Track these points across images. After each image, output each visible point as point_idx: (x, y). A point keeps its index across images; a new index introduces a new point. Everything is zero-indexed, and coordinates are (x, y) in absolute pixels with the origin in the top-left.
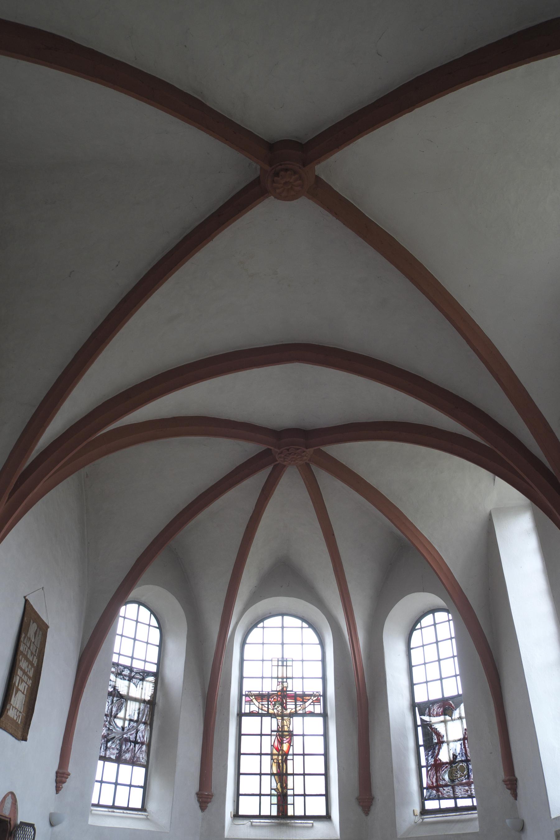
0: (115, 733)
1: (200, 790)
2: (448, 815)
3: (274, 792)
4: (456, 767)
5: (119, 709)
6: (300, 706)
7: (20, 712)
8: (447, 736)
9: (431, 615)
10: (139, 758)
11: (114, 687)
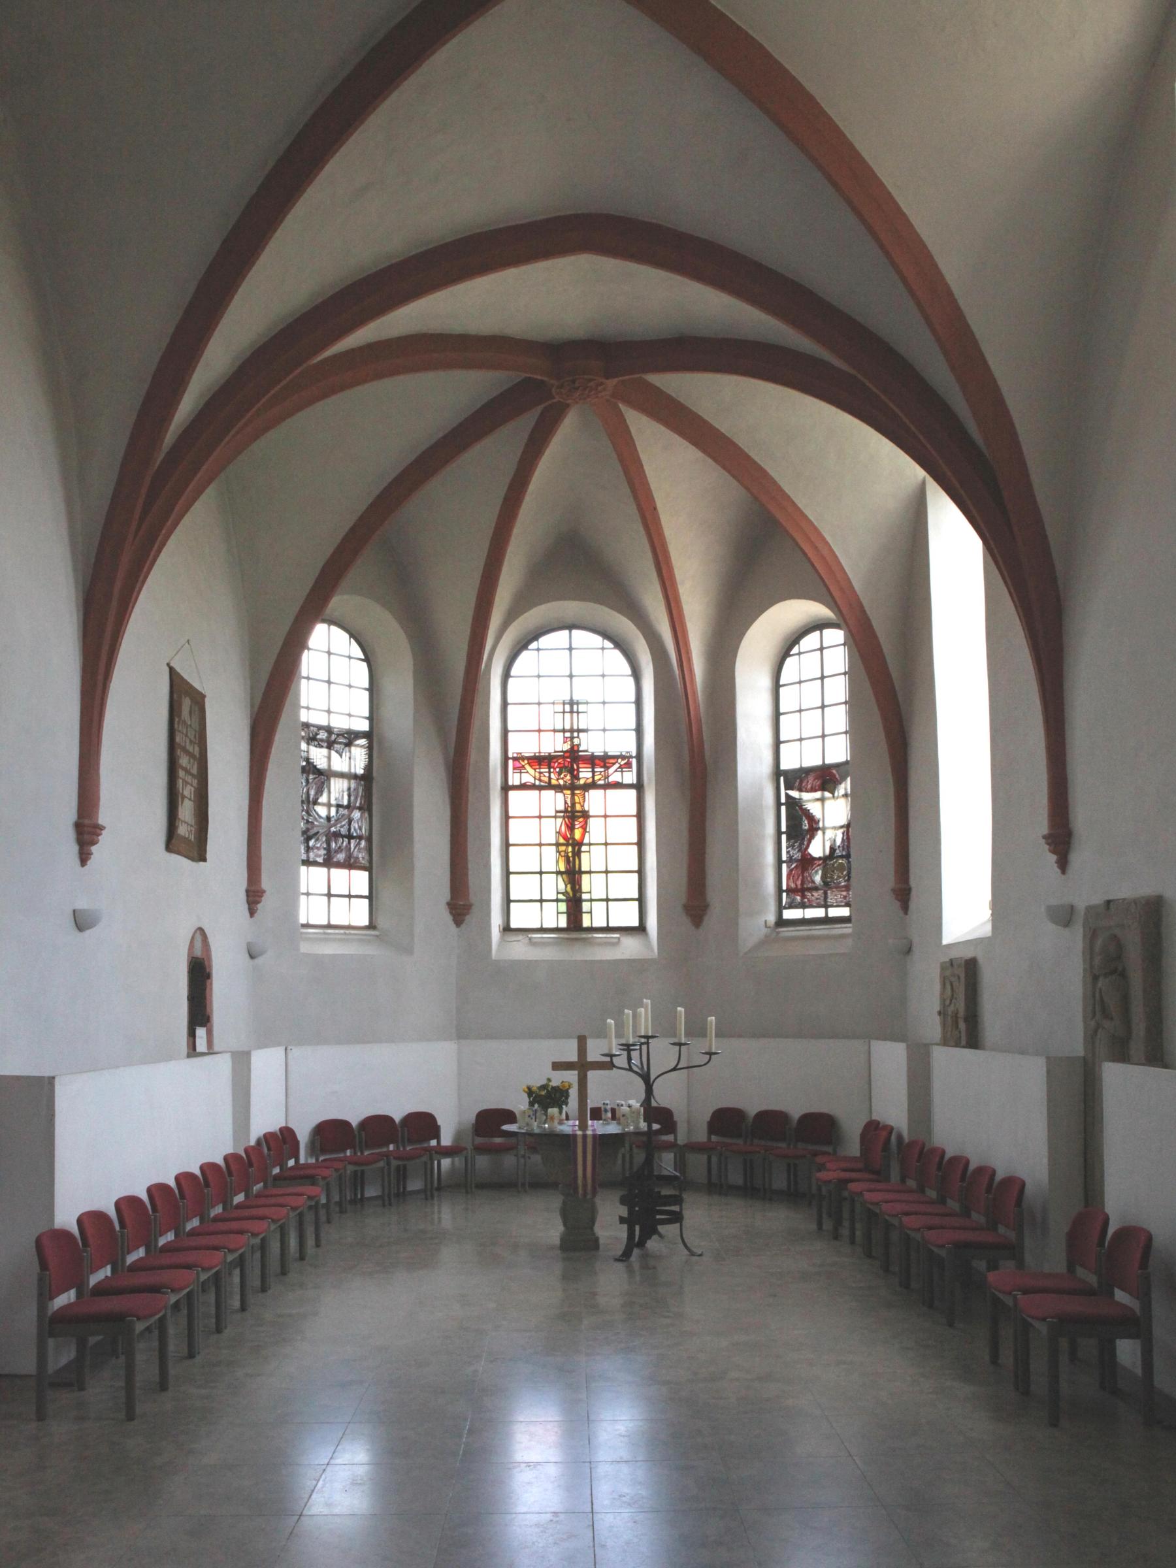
0: (317, 826)
1: (452, 898)
2: (814, 927)
3: (561, 897)
4: (833, 865)
5: (319, 792)
6: (600, 774)
7: (192, 826)
8: (823, 821)
9: (817, 633)
10: (358, 858)
11: (307, 760)
